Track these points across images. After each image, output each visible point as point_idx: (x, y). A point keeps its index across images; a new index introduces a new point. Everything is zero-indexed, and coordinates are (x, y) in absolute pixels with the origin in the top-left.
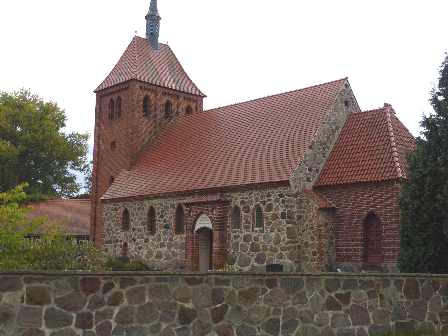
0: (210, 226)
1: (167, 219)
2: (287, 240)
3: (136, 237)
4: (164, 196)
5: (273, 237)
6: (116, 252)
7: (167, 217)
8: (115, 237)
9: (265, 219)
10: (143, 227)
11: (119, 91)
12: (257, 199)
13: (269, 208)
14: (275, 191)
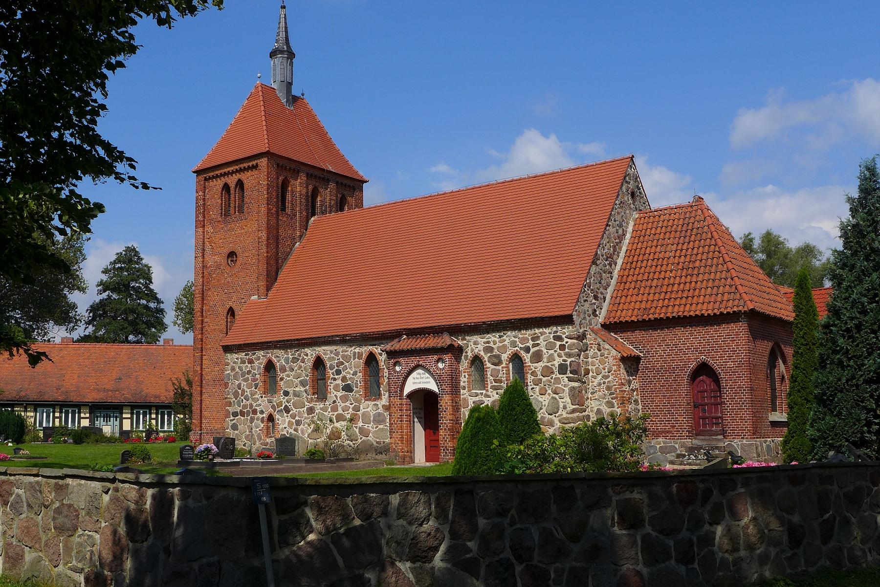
0: (433, 386)
1: (348, 376)
2: (571, 407)
3: (290, 405)
4: (344, 340)
5: (546, 403)
6: (254, 430)
7: (348, 373)
8: (251, 405)
9: (529, 376)
10: (302, 389)
11: (241, 170)
12: (514, 344)
13: (537, 357)
14: (547, 331)
